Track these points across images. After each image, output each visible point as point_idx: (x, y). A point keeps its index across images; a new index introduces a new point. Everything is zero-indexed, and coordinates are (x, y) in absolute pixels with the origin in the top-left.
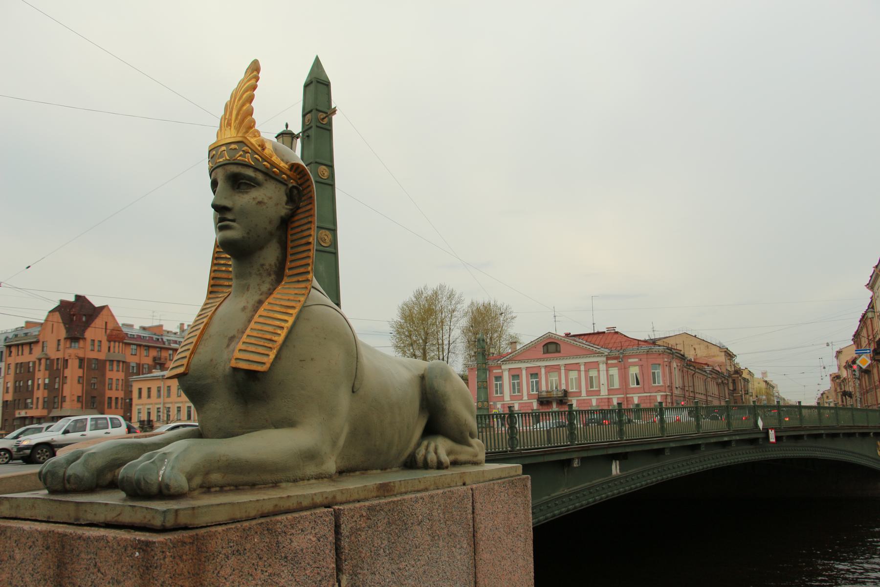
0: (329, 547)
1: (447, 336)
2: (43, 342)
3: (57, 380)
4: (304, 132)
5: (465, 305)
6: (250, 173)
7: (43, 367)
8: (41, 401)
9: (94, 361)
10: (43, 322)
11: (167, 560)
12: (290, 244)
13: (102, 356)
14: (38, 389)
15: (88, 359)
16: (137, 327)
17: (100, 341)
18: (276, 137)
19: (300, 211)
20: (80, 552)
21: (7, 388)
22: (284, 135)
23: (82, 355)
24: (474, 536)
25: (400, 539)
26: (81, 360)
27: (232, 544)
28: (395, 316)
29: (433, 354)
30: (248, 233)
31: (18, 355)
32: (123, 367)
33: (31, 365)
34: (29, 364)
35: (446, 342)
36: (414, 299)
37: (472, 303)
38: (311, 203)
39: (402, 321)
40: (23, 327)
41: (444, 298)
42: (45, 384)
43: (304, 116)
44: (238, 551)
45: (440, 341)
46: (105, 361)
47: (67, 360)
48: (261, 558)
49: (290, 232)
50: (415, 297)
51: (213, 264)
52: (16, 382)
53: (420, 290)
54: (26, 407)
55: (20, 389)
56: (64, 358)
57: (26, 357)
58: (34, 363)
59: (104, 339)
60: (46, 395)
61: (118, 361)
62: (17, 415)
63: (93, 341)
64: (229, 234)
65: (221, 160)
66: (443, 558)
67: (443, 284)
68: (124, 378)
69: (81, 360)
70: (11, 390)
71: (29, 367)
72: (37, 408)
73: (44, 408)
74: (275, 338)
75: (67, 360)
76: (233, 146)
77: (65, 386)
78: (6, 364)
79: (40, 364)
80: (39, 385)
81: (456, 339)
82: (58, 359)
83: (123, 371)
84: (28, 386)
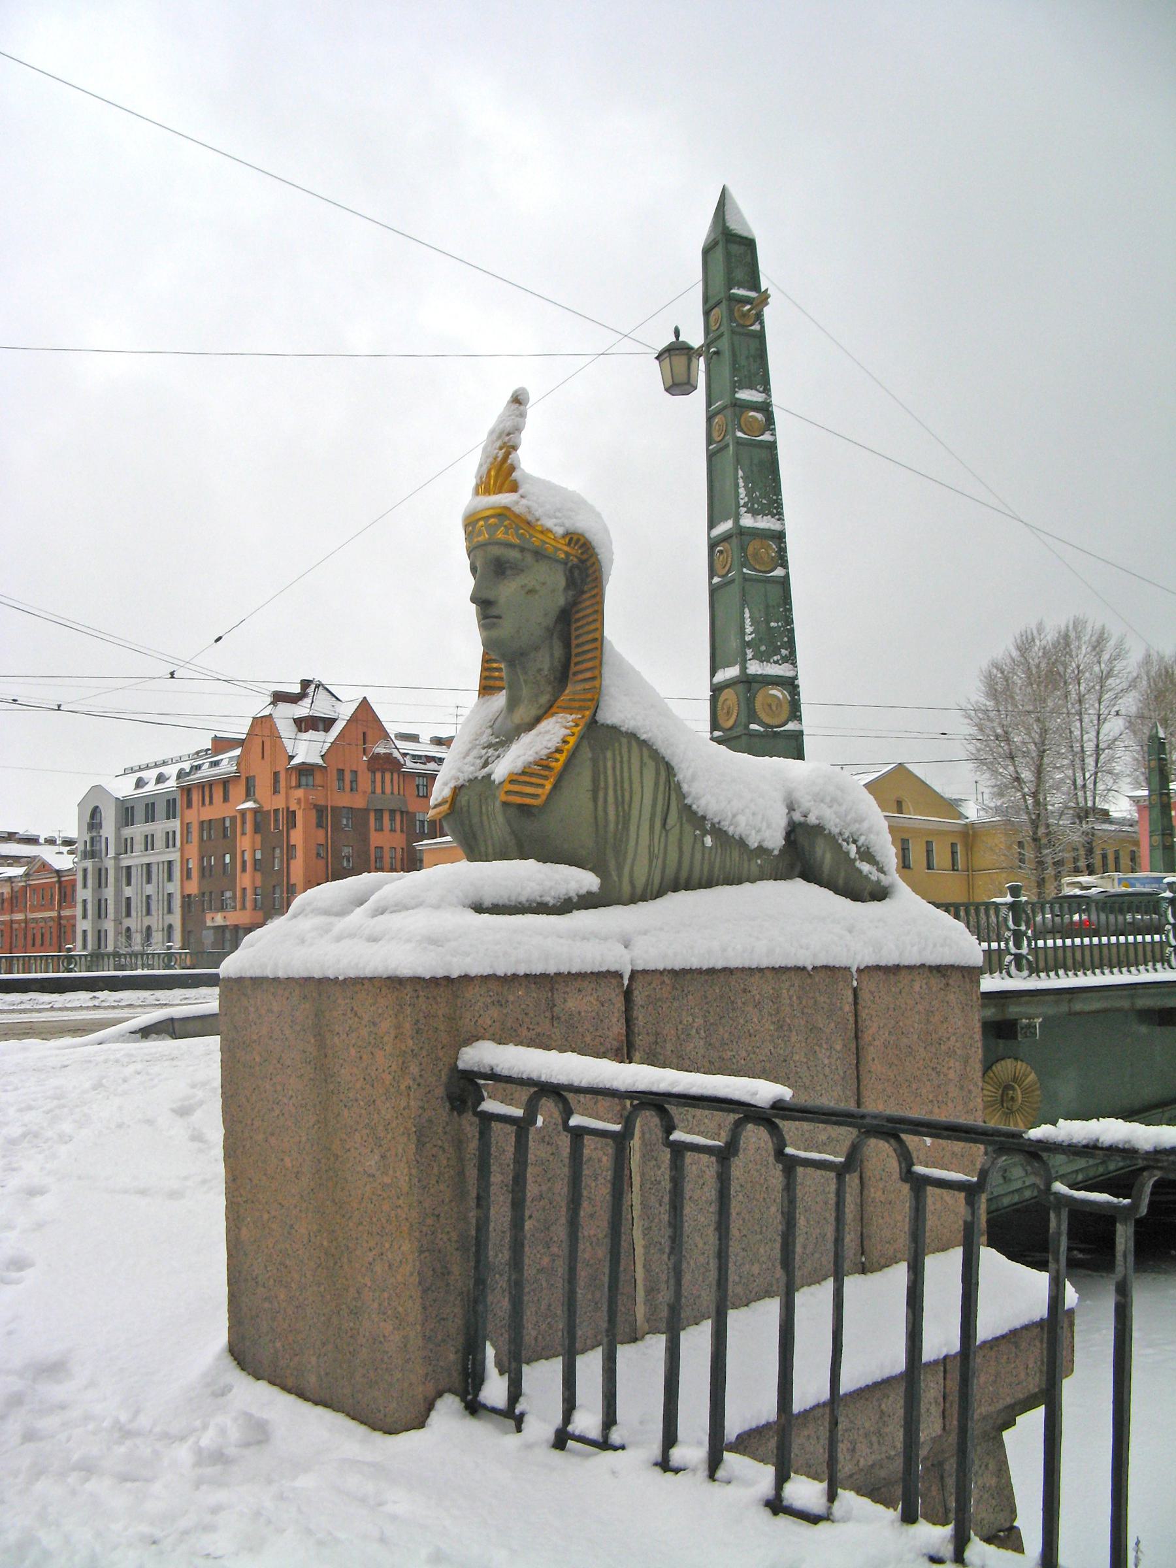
0: (616, 1015)
1: (1093, 734)
2: (247, 778)
3: (278, 851)
4: (708, 345)
5: (1131, 664)
6: (514, 554)
7: (249, 827)
8: (250, 896)
9: (345, 811)
10: (244, 737)
11: (420, 999)
12: (574, 642)
13: (359, 802)
14: (244, 870)
15: (334, 809)
16: (425, 737)
17: (355, 772)
18: (657, 358)
19: (585, 596)
20: (337, 999)
21: (189, 870)
22: (672, 352)
23: (322, 802)
24: (857, 1037)
25: (723, 1021)
26: (320, 811)
27: (491, 994)
28: (975, 693)
29: (1062, 775)
30: (518, 632)
31: (203, 804)
32: (402, 821)
33: (228, 824)
34: (224, 823)
35: (1090, 747)
36: (1015, 654)
37: (1148, 656)
38: (596, 587)
39: (990, 704)
40: (209, 750)
41: (1084, 648)
42: (255, 860)
43: (707, 313)
44: (498, 1002)
45: (1077, 749)
46: (366, 811)
47: (294, 812)
48: (526, 1014)
49: (574, 626)
50: (1019, 648)
51: (484, 669)
52: (203, 858)
53: (1029, 632)
54: (222, 908)
55: (211, 871)
56: (288, 808)
57: (216, 810)
58: (233, 819)
59: (362, 769)
60: (258, 883)
61: (392, 812)
62: (209, 923)
63: (341, 772)
64: (495, 633)
65: (480, 539)
66: (796, 1057)
67: (1081, 617)
68: (405, 847)
69: (320, 811)
70: (195, 874)
71: (225, 829)
72: (244, 907)
73: (255, 908)
74: (553, 764)
75: (294, 812)
76: (492, 520)
77: (293, 862)
78: (182, 823)
79: (244, 822)
80: (244, 863)
81: (1115, 740)
82: (276, 811)
83: (402, 831)
84: (225, 865)
